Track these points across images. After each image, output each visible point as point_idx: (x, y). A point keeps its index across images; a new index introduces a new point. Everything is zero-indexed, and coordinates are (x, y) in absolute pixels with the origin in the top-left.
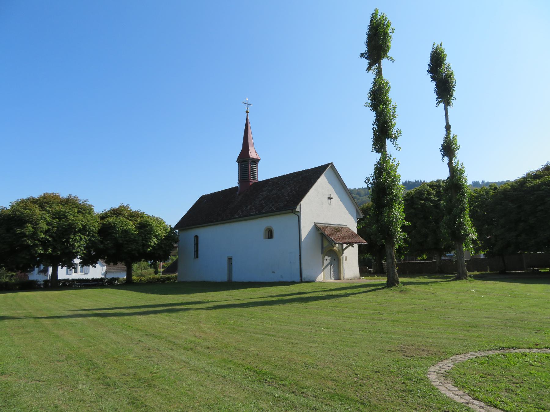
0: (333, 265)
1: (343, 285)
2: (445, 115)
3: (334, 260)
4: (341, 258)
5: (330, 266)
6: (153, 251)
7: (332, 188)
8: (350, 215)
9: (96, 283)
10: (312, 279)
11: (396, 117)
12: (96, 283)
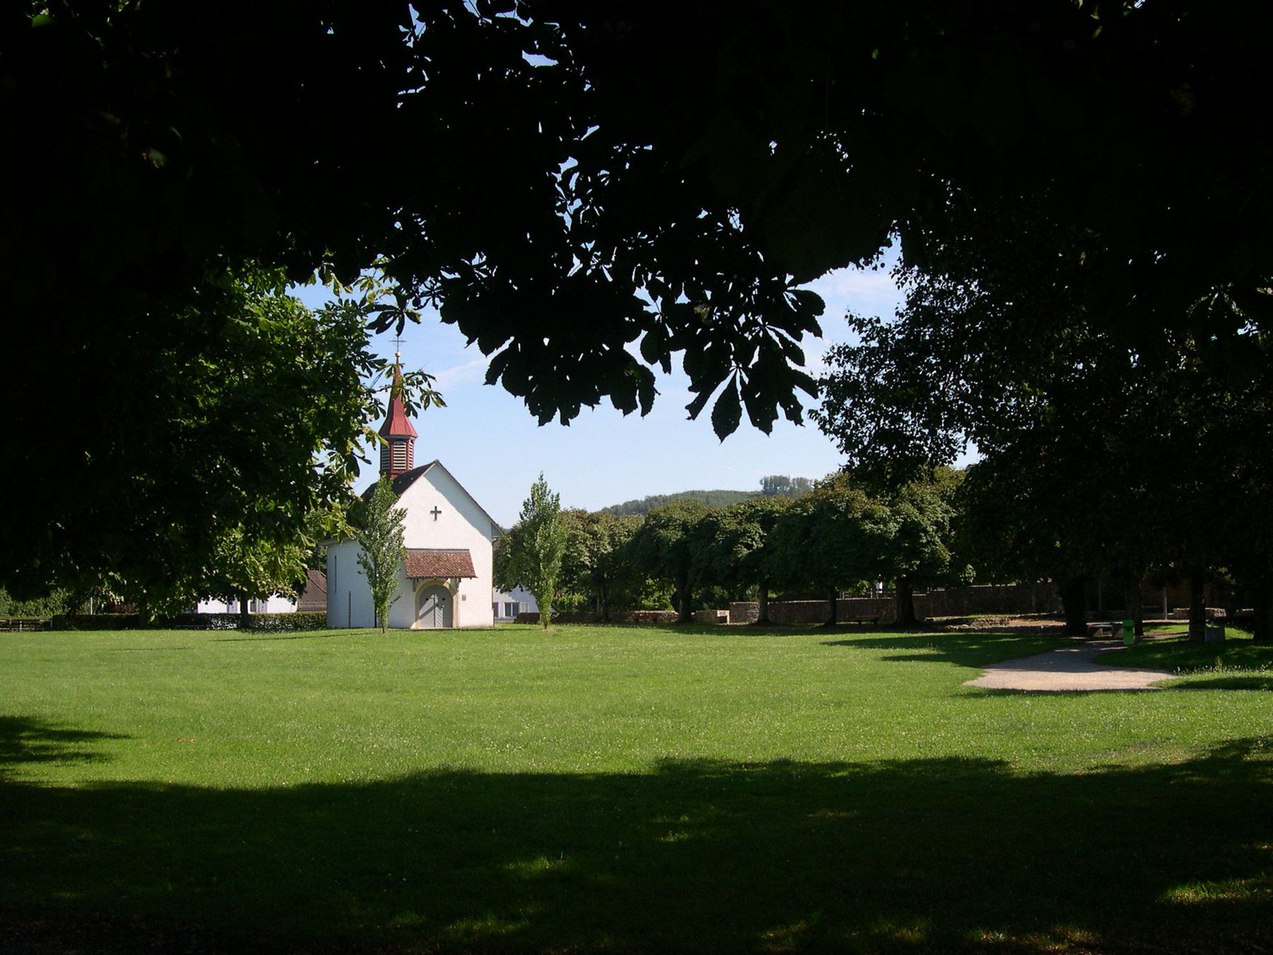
4: (454, 597)
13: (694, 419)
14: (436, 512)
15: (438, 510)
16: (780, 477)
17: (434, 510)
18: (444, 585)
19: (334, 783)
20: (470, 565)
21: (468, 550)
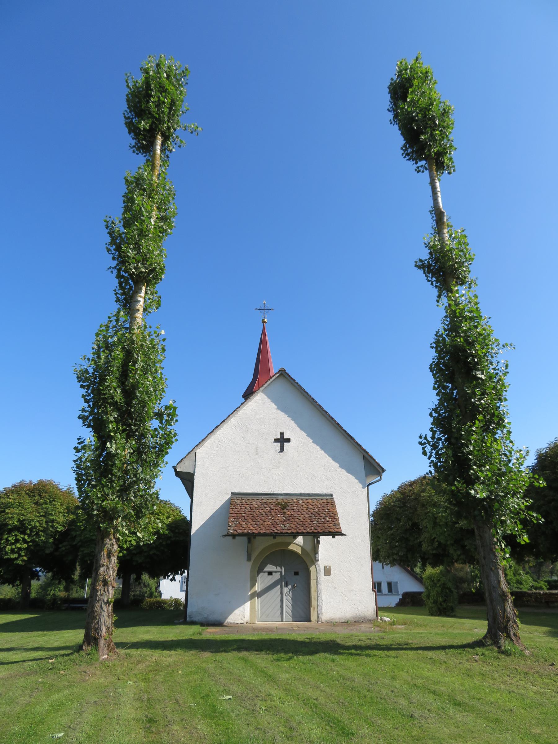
0: (290, 587)
1: (300, 637)
2: (431, 195)
3: (296, 574)
4: (312, 569)
5: (281, 587)
6: (128, 558)
7: (290, 419)
8: (344, 472)
9: (72, 605)
10: (212, 618)
11: (473, 259)
12: (72, 605)
13: (383, 470)
14: (282, 440)
15: (286, 437)
16: (401, 487)
17: (279, 437)
18: (291, 547)
19: (245, 621)
20: (334, 516)
21: (331, 495)
